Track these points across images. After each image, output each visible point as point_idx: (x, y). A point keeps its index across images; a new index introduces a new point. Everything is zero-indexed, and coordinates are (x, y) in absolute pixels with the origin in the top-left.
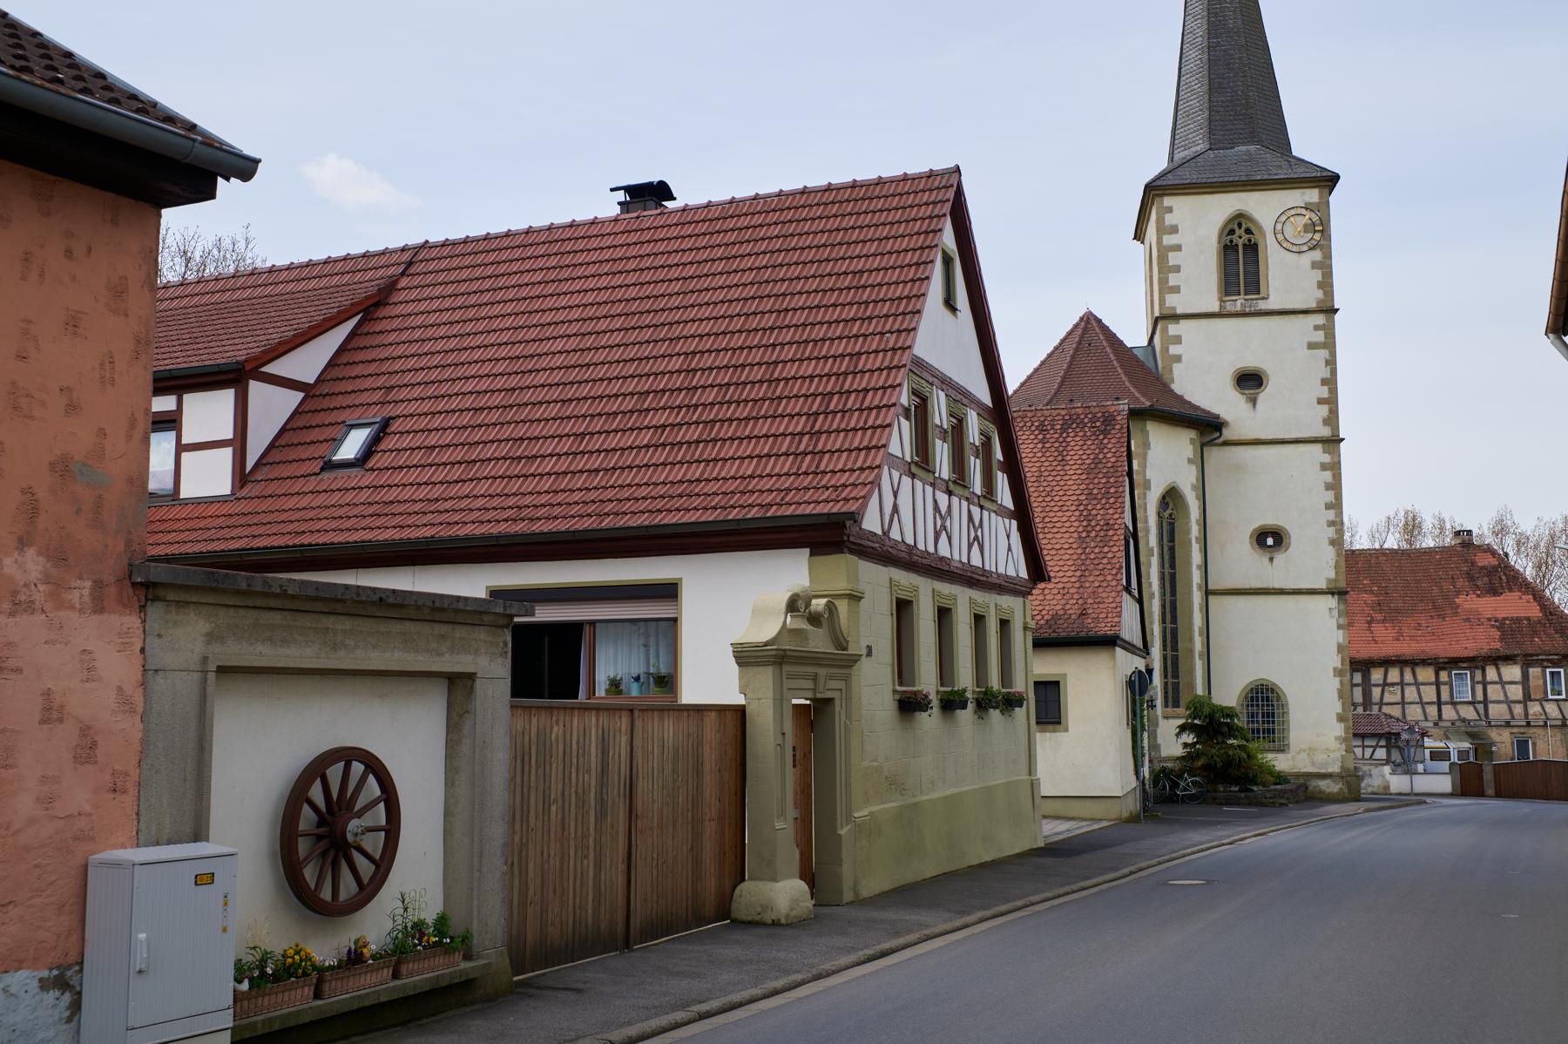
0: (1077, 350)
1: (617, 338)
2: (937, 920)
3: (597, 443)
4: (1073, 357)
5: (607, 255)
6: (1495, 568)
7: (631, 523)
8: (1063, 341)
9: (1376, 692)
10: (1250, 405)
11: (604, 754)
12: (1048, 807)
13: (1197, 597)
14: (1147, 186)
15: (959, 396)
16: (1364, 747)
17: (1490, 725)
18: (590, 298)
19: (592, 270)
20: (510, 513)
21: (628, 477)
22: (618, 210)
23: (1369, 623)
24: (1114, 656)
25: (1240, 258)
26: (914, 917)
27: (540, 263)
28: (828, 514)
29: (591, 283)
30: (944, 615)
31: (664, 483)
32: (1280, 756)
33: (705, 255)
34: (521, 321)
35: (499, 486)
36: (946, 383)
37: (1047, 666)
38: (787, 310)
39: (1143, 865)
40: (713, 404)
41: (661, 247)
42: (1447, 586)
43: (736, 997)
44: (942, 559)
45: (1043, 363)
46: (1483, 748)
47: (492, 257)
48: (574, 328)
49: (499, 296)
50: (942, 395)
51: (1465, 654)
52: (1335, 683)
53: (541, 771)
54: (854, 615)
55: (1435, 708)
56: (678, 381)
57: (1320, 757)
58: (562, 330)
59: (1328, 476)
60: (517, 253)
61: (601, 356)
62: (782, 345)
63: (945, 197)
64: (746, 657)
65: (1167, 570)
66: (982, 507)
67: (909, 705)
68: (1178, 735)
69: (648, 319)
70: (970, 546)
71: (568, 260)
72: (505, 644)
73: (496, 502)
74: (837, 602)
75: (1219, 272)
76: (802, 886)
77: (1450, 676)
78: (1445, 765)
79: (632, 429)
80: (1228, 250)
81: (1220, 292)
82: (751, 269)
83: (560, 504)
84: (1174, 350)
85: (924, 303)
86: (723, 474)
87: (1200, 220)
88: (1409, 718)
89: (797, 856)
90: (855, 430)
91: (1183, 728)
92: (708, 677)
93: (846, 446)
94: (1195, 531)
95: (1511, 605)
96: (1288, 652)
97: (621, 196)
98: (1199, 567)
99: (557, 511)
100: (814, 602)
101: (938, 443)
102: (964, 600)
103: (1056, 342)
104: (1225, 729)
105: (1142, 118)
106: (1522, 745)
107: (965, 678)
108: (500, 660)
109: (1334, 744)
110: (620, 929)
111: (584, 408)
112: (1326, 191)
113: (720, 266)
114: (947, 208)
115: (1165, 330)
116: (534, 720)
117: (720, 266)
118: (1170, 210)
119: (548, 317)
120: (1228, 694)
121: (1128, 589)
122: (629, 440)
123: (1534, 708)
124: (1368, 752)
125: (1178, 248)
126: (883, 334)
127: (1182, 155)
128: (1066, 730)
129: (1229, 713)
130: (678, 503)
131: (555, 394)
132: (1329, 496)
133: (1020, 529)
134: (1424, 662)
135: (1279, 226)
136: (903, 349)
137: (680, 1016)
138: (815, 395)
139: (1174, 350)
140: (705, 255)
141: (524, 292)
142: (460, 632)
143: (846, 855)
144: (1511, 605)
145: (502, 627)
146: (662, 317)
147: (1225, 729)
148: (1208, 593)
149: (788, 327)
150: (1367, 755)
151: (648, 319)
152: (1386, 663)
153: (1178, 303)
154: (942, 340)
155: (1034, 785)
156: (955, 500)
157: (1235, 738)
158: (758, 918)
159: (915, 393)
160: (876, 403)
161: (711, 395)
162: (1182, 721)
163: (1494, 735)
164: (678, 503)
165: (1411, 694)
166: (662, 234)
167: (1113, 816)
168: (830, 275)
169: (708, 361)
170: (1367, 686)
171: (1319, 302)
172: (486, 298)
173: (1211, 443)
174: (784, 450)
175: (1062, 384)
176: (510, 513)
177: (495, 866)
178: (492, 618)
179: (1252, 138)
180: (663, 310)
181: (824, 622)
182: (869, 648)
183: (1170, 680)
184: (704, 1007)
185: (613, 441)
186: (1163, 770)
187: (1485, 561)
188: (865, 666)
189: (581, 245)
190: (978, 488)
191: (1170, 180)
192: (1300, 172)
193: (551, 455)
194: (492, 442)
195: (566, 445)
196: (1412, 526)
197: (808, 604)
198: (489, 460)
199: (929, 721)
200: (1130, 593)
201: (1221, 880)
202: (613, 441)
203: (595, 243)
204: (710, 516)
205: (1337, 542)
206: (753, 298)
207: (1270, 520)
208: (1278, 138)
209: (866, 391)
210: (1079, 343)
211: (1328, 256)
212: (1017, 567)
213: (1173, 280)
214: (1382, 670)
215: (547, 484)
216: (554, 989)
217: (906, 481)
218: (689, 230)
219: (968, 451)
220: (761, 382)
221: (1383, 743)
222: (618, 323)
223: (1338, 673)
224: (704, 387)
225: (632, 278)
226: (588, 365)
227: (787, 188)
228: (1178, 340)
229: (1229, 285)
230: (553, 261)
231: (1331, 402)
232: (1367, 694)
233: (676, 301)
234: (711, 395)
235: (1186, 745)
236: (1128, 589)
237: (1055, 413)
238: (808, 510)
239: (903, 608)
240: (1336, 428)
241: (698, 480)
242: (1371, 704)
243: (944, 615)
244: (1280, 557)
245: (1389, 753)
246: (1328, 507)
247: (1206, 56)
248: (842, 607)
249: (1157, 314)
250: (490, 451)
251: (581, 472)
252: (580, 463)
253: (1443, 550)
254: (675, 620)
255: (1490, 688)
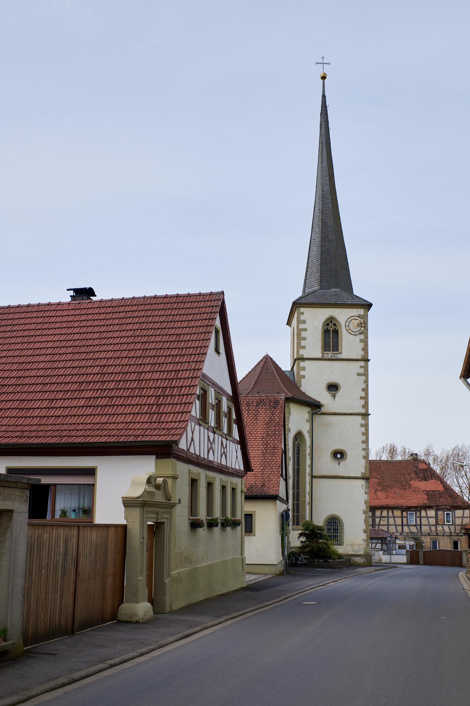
0: (261, 370)
1: (69, 357)
2: (207, 620)
3: (59, 404)
4: (260, 374)
5: (65, 319)
6: (426, 470)
7: (76, 441)
8: (256, 367)
9: (377, 520)
10: (333, 398)
11: (66, 546)
12: (248, 568)
13: (308, 479)
14: (293, 303)
15: (219, 391)
16: (372, 543)
17: (422, 535)
18: (57, 338)
19: (58, 325)
20: (18, 434)
21: (74, 420)
22: (69, 299)
23: (376, 491)
24: (276, 504)
25: (331, 336)
26: (197, 619)
27: (34, 320)
28: (165, 441)
29: (57, 331)
30: (210, 485)
31: (90, 424)
32: (340, 547)
33: (110, 322)
34: (25, 346)
35: (13, 421)
36: (215, 385)
37: (249, 507)
38: (147, 349)
39: (290, 595)
40: (113, 389)
41: (90, 317)
42: (407, 477)
43: (126, 657)
44: (210, 461)
45: (247, 376)
46: (419, 544)
47: (11, 316)
48: (49, 351)
49: (14, 334)
50: (213, 390)
51: (414, 505)
52: (363, 516)
53: (38, 554)
54: (174, 485)
55: (401, 527)
56: (97, 378)
57: (356, 548)
58: (44, 352)
59: (363, 429)
60: (23, 315)
61: (61, 364)
62: (145, 364)
63: (216, 305)
64: (128, 503)
65: (296, 467)
66: (227, 439)
67: (195, 525)
68: (299, 538)
69: (84, 349)
70: (221, 456)
71: (47, 320)
72: (27, 497)
73: (11, 428)
74: (167, 480)
75: (322, 341)
76: (149, 605)
77: (407, 514)
78: (404, 551)
79: (75, 398)
80: (326, 332)
81: (322, 349)
82: (131, 330)
83: (42, 431)
84: (302, 373)
85: (207, 350)
86: (117, 421)
87: (315, 318)
88: (390, 531)
89: (147, 590)
90: (177, 404)
91: (301, 535)
92: (109, 510)
93: (173, 411)
94: (308, 450)
95: (432, 485)
96: (344, 502)
97: (72, 293)
98: (309, 466)
99: (40, 434)
100: (158, 479)
101: (211, 411)
102: (218, 479)
103: (253, 367)
104: (319, 536)
105: (292, 272)
106: (434, 543)
107: (217, 514)
108: (24, 504)
109: (362, 542)
110: (70, 625)
111: (53, 388)
112: (367, 310)
113: (117, 328)
114: (218, 309)
115: (299, 364)
116: (36, 531)
117: (117, 328)
118: (303, 313)
119: (37, 345)
120: (319, 521)
121: (282, 475)
122: (74, 403)
123: (440, 528)
124: (374, 545)
125: (305, 330)
126: (189, 362)
127: (309, 290)
128: (254, 535)
129: (320, 529)
130: (97, 433)
131: (40, 380)
132: (364, 438)
133: (241, 449)
134: (397, 508)
135: (347, 324)
136: (198, 370)
137: (102, 666)
138: (159, 388)
139: (302, 373)
140: (110, 322)
141: (26, 333)
142: (7, 491)
143: (167, 591)
144: (432, 485)
145: (25, 489)
146: (90, 349)
147: (319, 536)
148: (312, 477)
149: (147, 357)
150: (373, 547)
151: (84, 349)
152: (382, 508)
153: (305, 353)
154: (213, 367)
155: (243, 560)
156: (216, 436)
157: (323, 539)
158: (130, 620)
159: (202, 389)
160: (186, 393)
161: (112, 385)
162: (301, 532)
163: (423, 539)
164: (97, 433)
165: (391, 521)
166: (90, 311)
167: (273, 573)
168: (166, 335)
169: (111, 370)
170: (374, 517)
171: (362, 356)
172: (8, 335)
173: (316, 413)
174: (145, 411)
175: (254, 385)
176: (18, 434)
177: (18, 597)
178: (22, 484)
179: (337, 285)
180: (90, 346)
181: (162, 488)
182: (180, 500)
183: (295, 514)
184: (113, 662)
185: (67, 403)
186: (292, 552)
187: (422, 466)
188: (178, 507)
189: (52, 314)
190: (225, 431)
191: (304, 301)
192: (356, 301)
193: (38, 408)
194: (10, 401)
195: (45, 404)
196: (393, 451)
197: (155, 480)
198: (9, 409)
199: (202, 532)
200: (282, 477)
201: (324, 602)
202: (67, 403)
203: (59, 313)
204: (112, 440)
205: (366, 457)
206: (132, 343)
207: (339, 447)
208: (349, 287)
209: (182, 387)
210: (263, 368)
211: (367, 337)
212: (239, 465)
213: (303, 343)
214: (380, 511)
215: (36, 421)
216: (42, 654)
217: (197, 427)
218: (103, 310)
219: (222, 414)
220: (135, 380)
221: (380, 542)
222: (70, 350)
223: (365, 512)
224: (109, 381)
225: (76, 330)
226: (56, 368)
227: (147, 295)
228: (304, 369)
229: (326, 347)
230: (40, 320)
231: (365, 398)
232: (374, 521)
233: (97, 342)
234: (112, 385)
235: (302, 542)
236: (282, 475)
237: (253, 398)
238: (156, 439)
239: (194, 482)
240: (367, 410)
241: (106, 423)
242: (375, 525)
243: (210, 485)
244: (342, 463)
245: (382, 546)
246: (363, 442)
247: (320, 250)
248: (170, 481)
249: (295, 357)
250: (9, 405)
251: (52, 416)
252: (51, 412)
253: (406, 462)
254: (93, 485)
255: (423, 519)
